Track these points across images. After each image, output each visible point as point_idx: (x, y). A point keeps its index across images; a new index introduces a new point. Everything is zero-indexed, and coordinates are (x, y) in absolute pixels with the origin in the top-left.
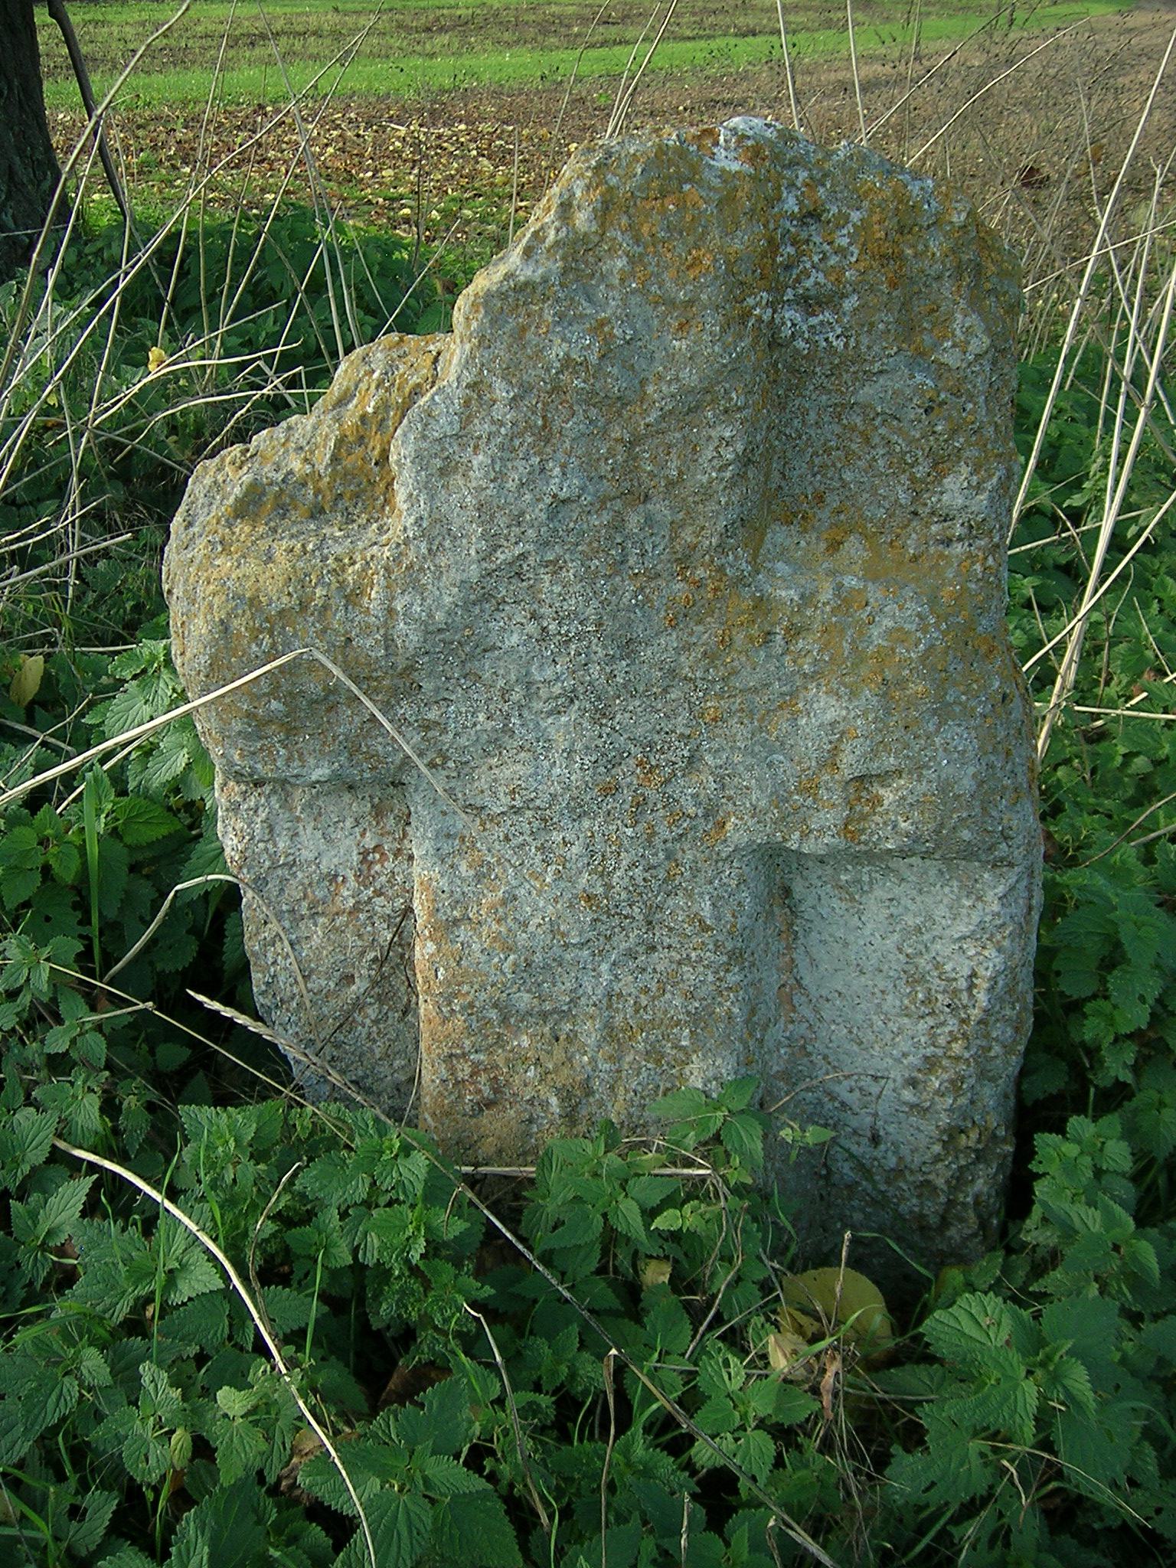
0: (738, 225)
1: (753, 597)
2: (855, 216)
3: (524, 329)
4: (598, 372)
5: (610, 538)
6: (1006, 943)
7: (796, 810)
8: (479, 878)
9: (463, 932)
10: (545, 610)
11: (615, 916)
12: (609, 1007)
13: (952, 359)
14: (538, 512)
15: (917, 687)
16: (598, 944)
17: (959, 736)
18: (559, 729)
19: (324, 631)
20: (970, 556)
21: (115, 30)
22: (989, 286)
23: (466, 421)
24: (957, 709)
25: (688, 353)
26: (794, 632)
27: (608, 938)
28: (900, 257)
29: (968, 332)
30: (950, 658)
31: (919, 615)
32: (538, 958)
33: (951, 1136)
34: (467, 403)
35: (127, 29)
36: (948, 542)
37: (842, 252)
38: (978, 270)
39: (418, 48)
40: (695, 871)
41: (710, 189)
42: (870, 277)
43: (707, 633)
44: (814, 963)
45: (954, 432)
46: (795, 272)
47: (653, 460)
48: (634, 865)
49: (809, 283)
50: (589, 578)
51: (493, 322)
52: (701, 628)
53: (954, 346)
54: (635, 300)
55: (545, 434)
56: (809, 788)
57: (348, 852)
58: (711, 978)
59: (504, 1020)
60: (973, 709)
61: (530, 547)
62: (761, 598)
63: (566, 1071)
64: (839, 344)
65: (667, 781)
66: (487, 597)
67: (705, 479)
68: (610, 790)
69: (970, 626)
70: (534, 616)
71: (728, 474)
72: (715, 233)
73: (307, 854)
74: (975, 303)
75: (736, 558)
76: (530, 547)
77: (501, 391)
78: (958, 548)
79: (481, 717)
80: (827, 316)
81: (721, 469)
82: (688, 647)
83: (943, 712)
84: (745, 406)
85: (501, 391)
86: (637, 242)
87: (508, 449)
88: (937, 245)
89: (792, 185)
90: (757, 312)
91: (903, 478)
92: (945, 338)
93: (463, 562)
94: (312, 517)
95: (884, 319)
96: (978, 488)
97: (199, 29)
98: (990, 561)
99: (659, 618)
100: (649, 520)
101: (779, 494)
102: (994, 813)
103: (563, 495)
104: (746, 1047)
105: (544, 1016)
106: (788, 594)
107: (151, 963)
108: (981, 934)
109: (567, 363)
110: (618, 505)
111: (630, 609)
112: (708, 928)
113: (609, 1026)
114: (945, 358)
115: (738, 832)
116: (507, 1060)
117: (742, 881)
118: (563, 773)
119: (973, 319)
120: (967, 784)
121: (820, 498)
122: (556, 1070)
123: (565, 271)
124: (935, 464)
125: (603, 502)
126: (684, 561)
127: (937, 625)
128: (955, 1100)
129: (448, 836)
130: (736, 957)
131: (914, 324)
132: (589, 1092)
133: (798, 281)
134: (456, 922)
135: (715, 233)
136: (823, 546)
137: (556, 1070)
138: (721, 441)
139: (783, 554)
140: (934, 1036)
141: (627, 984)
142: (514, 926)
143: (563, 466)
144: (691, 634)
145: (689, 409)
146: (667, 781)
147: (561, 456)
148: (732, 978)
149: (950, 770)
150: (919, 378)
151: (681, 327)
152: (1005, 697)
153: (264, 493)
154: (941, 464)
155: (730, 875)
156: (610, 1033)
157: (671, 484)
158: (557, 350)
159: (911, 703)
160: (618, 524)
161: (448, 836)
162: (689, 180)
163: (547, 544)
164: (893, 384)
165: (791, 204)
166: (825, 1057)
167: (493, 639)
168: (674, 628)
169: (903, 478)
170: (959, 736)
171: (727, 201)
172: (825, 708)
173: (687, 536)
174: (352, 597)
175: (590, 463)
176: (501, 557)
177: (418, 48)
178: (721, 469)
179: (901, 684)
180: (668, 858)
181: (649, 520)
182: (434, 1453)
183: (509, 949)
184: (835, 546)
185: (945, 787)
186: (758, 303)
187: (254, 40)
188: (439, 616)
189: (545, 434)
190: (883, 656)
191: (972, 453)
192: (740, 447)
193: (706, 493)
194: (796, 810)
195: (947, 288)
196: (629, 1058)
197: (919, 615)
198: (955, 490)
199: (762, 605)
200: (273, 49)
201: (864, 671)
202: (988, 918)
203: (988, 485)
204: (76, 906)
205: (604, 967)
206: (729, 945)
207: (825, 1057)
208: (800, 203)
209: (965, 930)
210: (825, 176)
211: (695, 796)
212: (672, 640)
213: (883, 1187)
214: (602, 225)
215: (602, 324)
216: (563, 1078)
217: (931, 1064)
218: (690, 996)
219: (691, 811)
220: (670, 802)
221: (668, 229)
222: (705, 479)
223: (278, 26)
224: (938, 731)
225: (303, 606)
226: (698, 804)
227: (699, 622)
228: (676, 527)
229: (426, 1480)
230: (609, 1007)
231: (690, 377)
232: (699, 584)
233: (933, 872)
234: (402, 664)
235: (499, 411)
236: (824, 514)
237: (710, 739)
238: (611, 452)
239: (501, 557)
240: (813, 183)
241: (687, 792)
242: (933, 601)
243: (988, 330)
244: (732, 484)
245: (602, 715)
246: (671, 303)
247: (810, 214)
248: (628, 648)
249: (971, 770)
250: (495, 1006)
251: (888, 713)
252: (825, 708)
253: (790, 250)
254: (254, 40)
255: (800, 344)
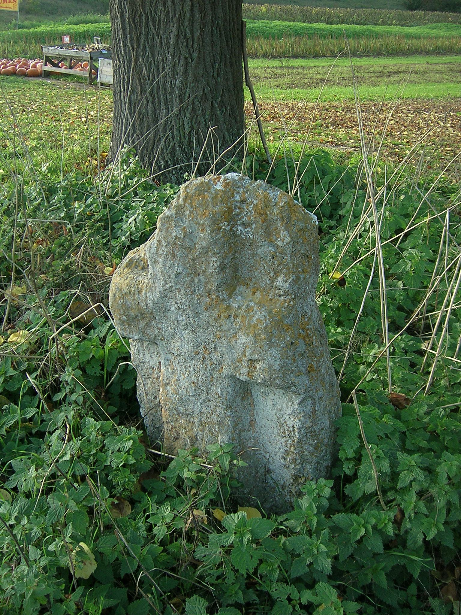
0: (217, 204)
1: (226, 305)
2: (255, 202)
3: (168, 228)
4: (183, 241)
5: (191, 284)
6: (302, 419)
7: (237, 366)
8: (173, 373)
9: (169, 387)
10: (178, 302)
11: (201, 389)
12: (201, 415)
13: (280, 243)
14: (173, 276)
15: (263, 336)
16: (197, 396)
17: (275, 352)
18: (186, 333)
19: (134, 299)
20: (285, 300)
21: (340, 69)
22: (293, 223)
23: (158, 250)
24: (275, 344)
25: (203, 238)
26: (236, 316)
27: (199, 395)
28: (266, 214)
29: (284, 236)
30: (273, 329)
31: (264, 316)
32: (183, 398)
33: (296, 478)
34: (157, 245)
35: (345, 68)
36: (280, 296)
37: (250, 211)
38: (289, 218)
39: (454, 79)
40: (217, 380)
41: (212, 194)
42: (257, 219)
43: (215, 313)
44: (257, 414)
45: (279, 265)
46: (240, 216)
47: (199, 265)
48: (203, 376)
49: (244, 220)
50: (186, 294)
51: (162, 225)
52: (213, 312)
53: (281, 240)
54: (192, 222)
55: (174, 255)
56: (240, 361)
57: (156, 361)
58: (223, 412)
59: (178, 414)
60: (280, 345)
61: (173, 284)
62: (229, 306)
63: (191, 432)
64: (252, 237)
65: (210, 353)
66: (166, 296)
67: (211, 271)
68: (197, 353)
69: (281, 321)
70: (176, 303)
71: (217, 271)
72: (211, 206)
73: (147, 360)
74: (286, 228)
75: (222, 293)
76: (173, 284)
77: (164, 243)
78: (282, 298)
79: (169, 328)
80: (249, 229)
81: (215, 269)
82: (211, 316)
83: (270, 345)
84: (219, 253)
85: (164, 243)
86: (192, 207)
87: (166, 258)
88: (276, 211)
89: (238, 193)
90: (224, 227)
91: (268, 276)
92: (279, 238)
93: (159, 287)
94: (142, 269)
95: (261, 231)
96: (286, 282)
97: (372, 69)
98: (292, 303)
99: (203, 308)
100: (199, 280)
101: (234, 276)
102: (288, 377)
103: (178, 271)
104: (232, 435)
105: (187, 415)
106: (235, 305)
107: (122, 386)
108: (293, 413)
109: (176, 237)
110: (192, 276)
111: (196, 304)
112: (220, 397)
113: (200, 421)
114: (278, 243)
115: (226, 371)
116: (179, 426)
117: (229, 385)
118: (188, 347)
119: (285, 233)
120: (276, 367)
121: (251, 279)
122: (189, 431)
123: (176, 214)
124: (275, 273)
125: (188, 275)
126: (209, 293)
127: (269, 319)
128: (295, 466)
129: (167, 360)
130: (228, 407)
131: (269, 233)
132: (197, 440)
133: (241, 219)
134: (168, 384)
135: (211, 206)
136: (251, 293)
137: (189, 431)
138: (214, 262)
139: (241, 294)
140: (286, 444)
141: (204, 410)
142: (179, 388)
143: (178, 264)
144: (211, 313)
145: (206, 252)
146: (210, 353)
147: (177, 261)
148: (228, 413)
149: (272, 362)
150: (270, 248)
151: (202, 230)
152: (292, 343)
153: (133, 262)
154: (277, 274)
155: (226, 383)
156: (201, 423)
157: (204, 272)
158: (174, 234)
159: (262, 340)
160: (192, 281)
161: (167, 360)
162: (206, 192)
163: (176, 284)
164: (265, 250)
165: (238, 198)
166: (263, 445)
167: (168, 308)
168: (207, 310)
169: (268, 276)
170: (275, 352)
171: (215, 197)
172: (243, 339)
173: (209, 286)
174: (140, 292)
175: (184, 264)
176: (167, 286)
177: (454, 79)
178: (215, 269)
179: (259, 335)
180: (211, 375)
181: (199, 280)
182: (72, 499)
183: (177, 394)
184: (254, 293)
185: (270, 366)
186: (224, 225)
187: (390, 74)
188: (156, 299)
189: (174, 255)
190: (255, 326)
191: (285, 271)
192: (218, 264)
193: (212, 275)
194: (237, 366)
195: (279, 223)
196: (205, 432)
197: (264, 316)
198: (280, 281)
199: (228, 307)
200: (396, 78)
201: (251, 329)
202: (295, 410)
203: (289, 281)
204: (101, 365)
205: (199, 404)
206: (226, 403)
207: (263, 445)
208: (240, 198)
209: (290, 412)
210: (248, 190)
211: (216, 358)
212: (206, 314)
213: (281, 490)
214: (185, 202)
215: (185, 228)
216: (190, 434)
217: (287, 453)
218: (218, 416)
219: (215, 363)
220: (211, 359)
221: (199, 205)
222: (211, 271)
223: (403, 68)
224: (268, 350)
225: (130, 292)
226: (217, 361)
227: (213, 310)
228: (206, 284)
229: (68, 505)
230: (201, 415)
231: (204, 244)
232: (213, 299)
233: (281, 393)
234: (150, 311)
235: (164, 248)
236: (251, 284)
237: (219, 343)
238: (189, 262)
239: (167, 286)
240: (244, 192)
241: (215, 356)
242: (270, 312)
243: (290, 236)
244: (219, 273)
245: (194, 332)
246: (199, 224)
247: (243, 201)
248: (197, 315)
249: (278, 363)
250: (175, 409)
251: (256, 342)
252: (243, 339)
253: (238, 210)
254: (390, 74)
255: (243, 236)
